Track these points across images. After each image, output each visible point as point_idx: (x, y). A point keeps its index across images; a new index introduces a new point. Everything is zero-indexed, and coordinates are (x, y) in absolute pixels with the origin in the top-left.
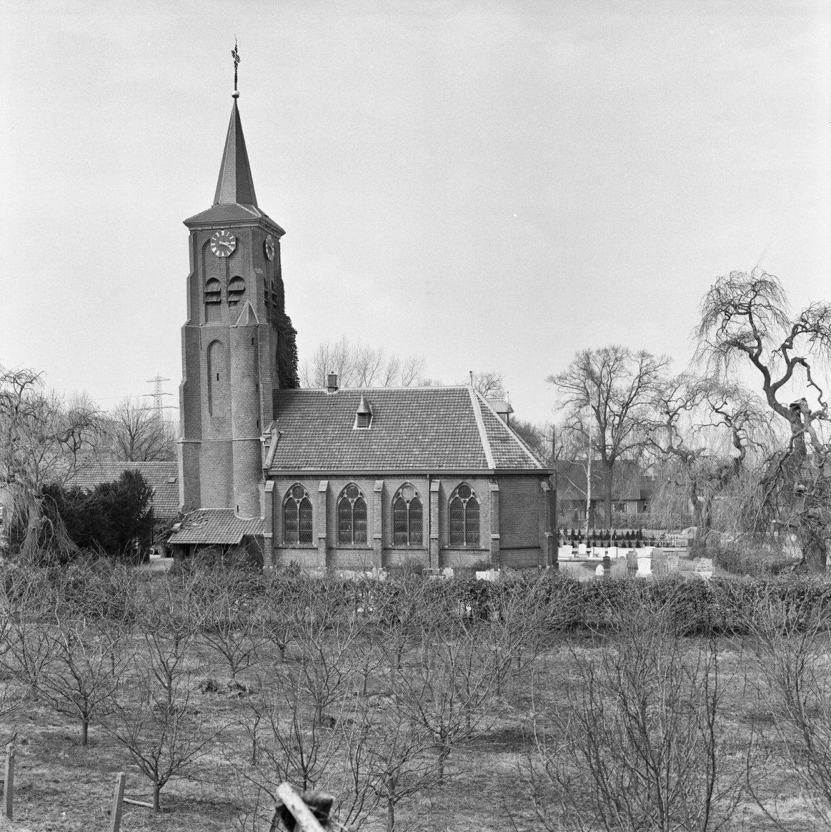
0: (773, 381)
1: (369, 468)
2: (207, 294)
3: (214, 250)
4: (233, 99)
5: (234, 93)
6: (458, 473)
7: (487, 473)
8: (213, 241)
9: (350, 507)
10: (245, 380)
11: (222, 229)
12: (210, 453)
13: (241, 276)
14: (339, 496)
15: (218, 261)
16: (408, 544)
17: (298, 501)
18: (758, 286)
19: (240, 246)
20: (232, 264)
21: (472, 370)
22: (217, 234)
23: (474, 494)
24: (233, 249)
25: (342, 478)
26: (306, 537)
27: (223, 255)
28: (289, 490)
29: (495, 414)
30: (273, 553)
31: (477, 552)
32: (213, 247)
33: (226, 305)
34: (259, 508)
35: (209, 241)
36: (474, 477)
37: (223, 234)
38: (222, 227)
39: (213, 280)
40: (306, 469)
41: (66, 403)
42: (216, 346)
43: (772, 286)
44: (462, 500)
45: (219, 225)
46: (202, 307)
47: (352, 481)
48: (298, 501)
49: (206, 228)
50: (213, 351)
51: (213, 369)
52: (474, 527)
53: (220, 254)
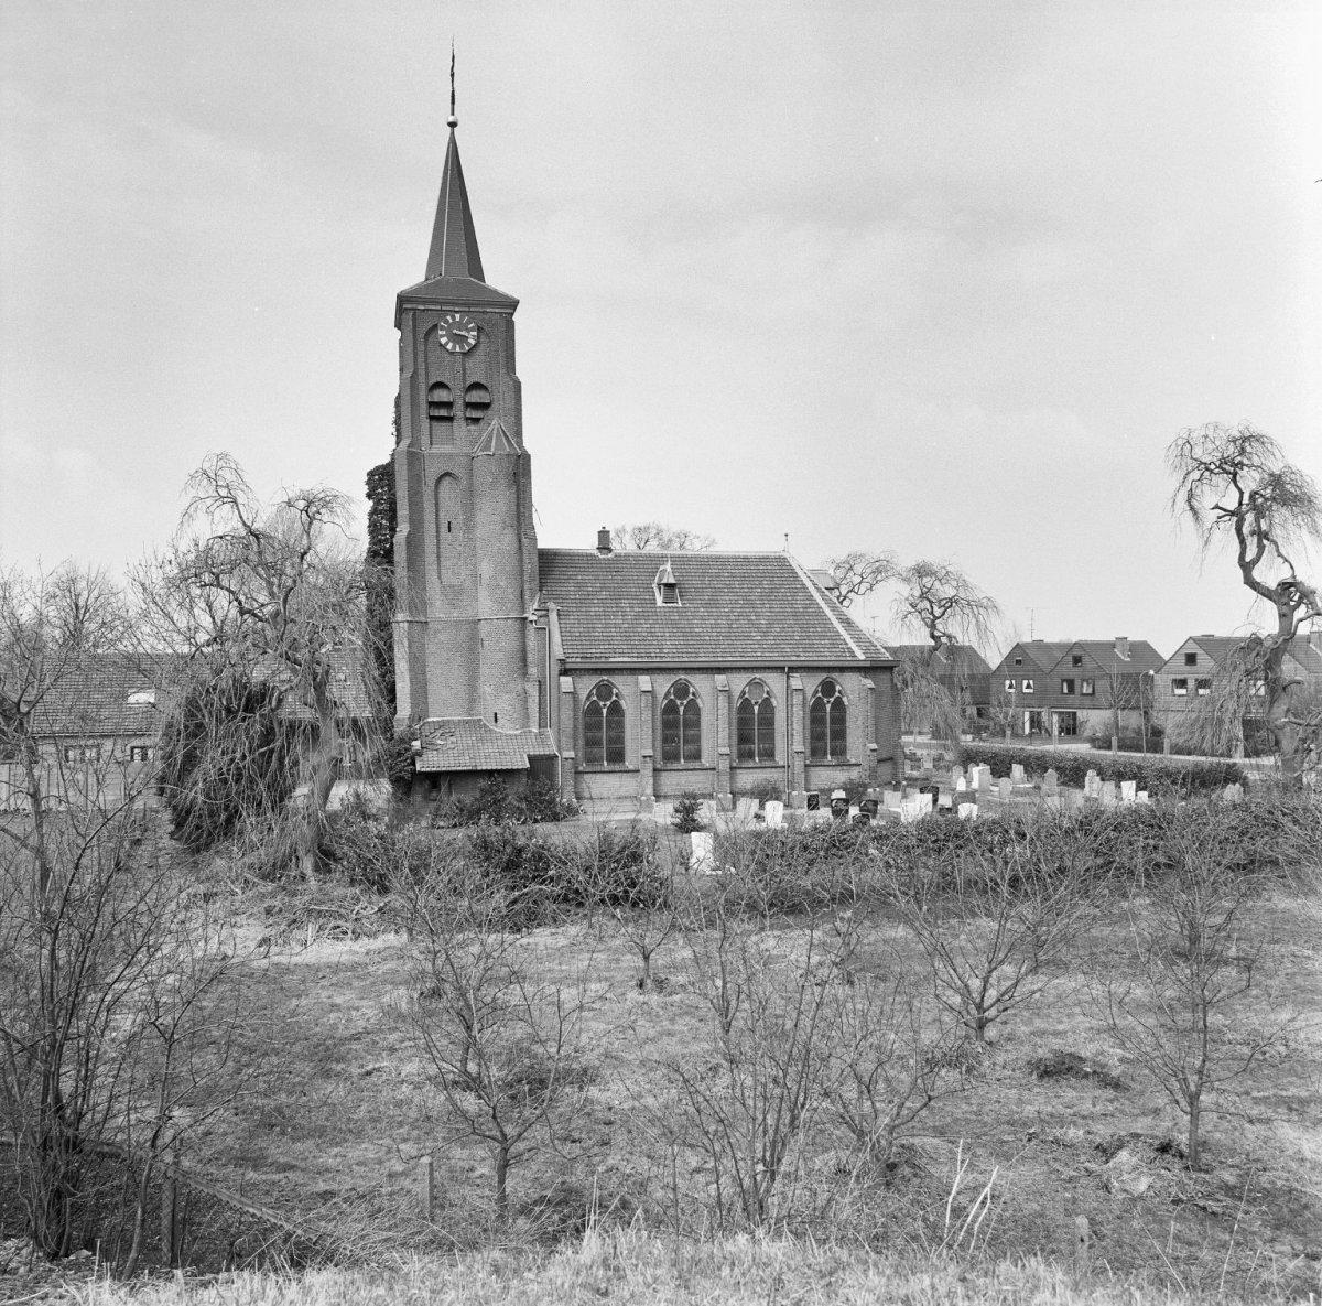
0: (1248, 559)
1: (704, 658)
2: (432, 404)
3: (444, 340)
4: (449, 128)
5: (451, 119)
6: (820, 664)
7: (855, 664)
8: (442, 328)
9: (677, 712)
10: (506, 531)
11: (457, 312)
12: (442, 637)
13: (484, 382)
14: (740, 697)
15: (449, 358)
16: (757, 759)
18: (1244, 441)
19: (483, 338)
20: (470, 363)
21: (788, 532)
22: (449, 318)
24: (473, 342)
26: (617, 756)
27: (458, 350)
30: (654, 777)
31: (845, 768)
32: (442, 336)
34: (527, 716)
35: (435, 327)
36: (842, 670)
37: (458, 319)
38: (457, 309)
39: (440, 385)
40: (615, 660)
41: (627, 538)
43: (1258, 439)
44: (825, 700)
45: (454, 304)
46: (425, 424)
47: (605, 678)
49: (433, 307)
50: (441, 488)
51: (442, 514)
52: (840, 734)
53: (454, 347)
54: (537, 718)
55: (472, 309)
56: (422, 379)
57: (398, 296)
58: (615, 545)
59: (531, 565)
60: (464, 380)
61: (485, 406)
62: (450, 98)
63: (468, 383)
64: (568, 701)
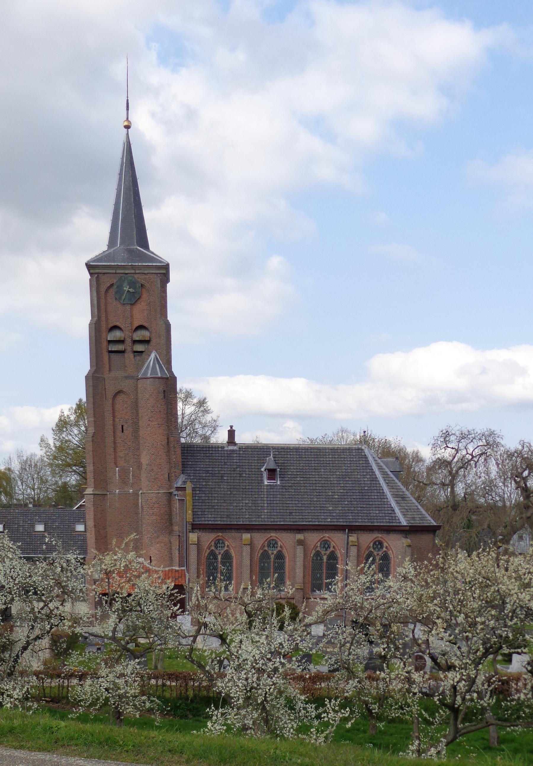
4: (125, 130)
5: (126, 123)
9: (269, 558)
13: (145, 324)
17: (273, 553)
23: (386, 547)
25: (263, 531)
28: (211, 542)
29: (389, 473)
33: (131, 355)
39: (115, 327)
42: (120, 398)
46: (106, 356)
47: (272, 534)
48: (378, 554)
54: (178, 561)
55: (137, 272)
56: (103, 323)
57: (86, 264)
58: (238, 440)
59: (177, 456)
60: (131, 324)
61: (147, 342)
62: (126, 105)
63: (134, 328)
64: (246, 550)
